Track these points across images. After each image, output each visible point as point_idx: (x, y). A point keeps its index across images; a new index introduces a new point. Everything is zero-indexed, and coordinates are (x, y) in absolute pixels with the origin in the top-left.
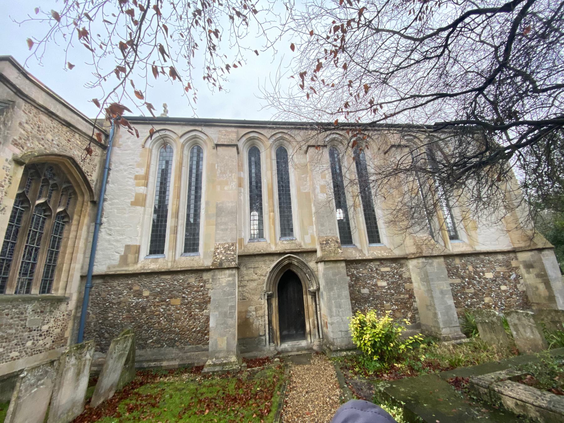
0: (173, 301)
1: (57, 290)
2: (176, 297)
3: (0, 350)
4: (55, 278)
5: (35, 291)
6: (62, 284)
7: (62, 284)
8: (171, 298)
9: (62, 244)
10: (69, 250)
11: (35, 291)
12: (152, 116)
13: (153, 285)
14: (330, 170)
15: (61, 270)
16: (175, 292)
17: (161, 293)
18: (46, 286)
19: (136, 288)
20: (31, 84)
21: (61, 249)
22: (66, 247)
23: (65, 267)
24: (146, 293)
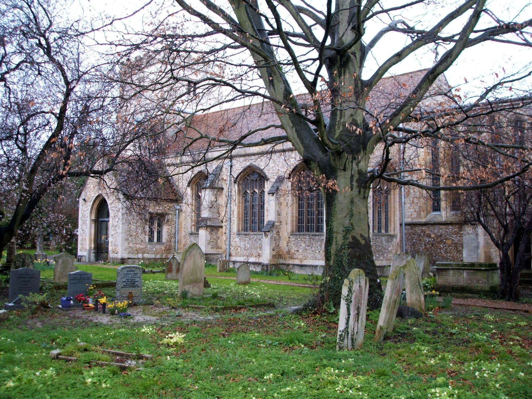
0: (447, 242)
1: (391, 231)
2: (449, 239)
3: (4, 7)
4: (389, 225)
5: (383, 231)
6: (392, 228)
7: (392, 228)
8: (446, 239)
9: (389, 206)
10: (392, 210)
11: (383, 231)
12: (475, 29)
13: (436, 231)
14: (458, 7)
15: (391, 221)
16: (448, 236)
17: (440, 236)
18: (387, 230)
19: (427, 232)
20: (523, 79)
21: (389, 209)
22: (391, 208)
23: (392, 219)
24: (433, 236)
